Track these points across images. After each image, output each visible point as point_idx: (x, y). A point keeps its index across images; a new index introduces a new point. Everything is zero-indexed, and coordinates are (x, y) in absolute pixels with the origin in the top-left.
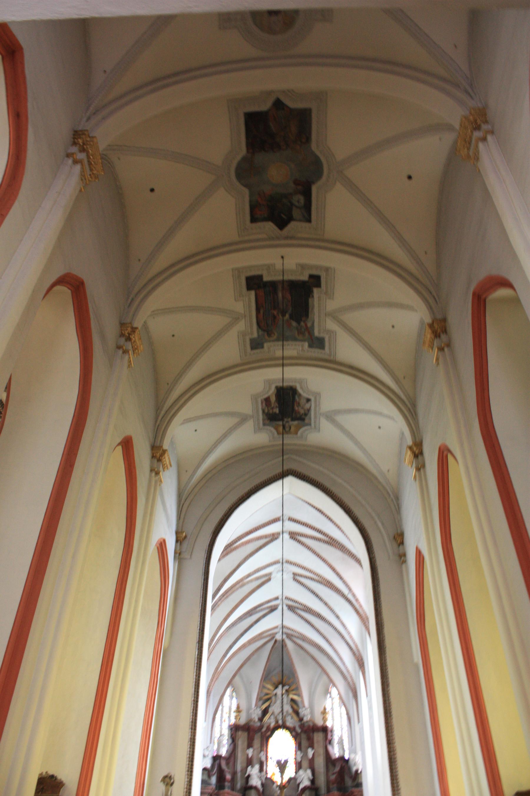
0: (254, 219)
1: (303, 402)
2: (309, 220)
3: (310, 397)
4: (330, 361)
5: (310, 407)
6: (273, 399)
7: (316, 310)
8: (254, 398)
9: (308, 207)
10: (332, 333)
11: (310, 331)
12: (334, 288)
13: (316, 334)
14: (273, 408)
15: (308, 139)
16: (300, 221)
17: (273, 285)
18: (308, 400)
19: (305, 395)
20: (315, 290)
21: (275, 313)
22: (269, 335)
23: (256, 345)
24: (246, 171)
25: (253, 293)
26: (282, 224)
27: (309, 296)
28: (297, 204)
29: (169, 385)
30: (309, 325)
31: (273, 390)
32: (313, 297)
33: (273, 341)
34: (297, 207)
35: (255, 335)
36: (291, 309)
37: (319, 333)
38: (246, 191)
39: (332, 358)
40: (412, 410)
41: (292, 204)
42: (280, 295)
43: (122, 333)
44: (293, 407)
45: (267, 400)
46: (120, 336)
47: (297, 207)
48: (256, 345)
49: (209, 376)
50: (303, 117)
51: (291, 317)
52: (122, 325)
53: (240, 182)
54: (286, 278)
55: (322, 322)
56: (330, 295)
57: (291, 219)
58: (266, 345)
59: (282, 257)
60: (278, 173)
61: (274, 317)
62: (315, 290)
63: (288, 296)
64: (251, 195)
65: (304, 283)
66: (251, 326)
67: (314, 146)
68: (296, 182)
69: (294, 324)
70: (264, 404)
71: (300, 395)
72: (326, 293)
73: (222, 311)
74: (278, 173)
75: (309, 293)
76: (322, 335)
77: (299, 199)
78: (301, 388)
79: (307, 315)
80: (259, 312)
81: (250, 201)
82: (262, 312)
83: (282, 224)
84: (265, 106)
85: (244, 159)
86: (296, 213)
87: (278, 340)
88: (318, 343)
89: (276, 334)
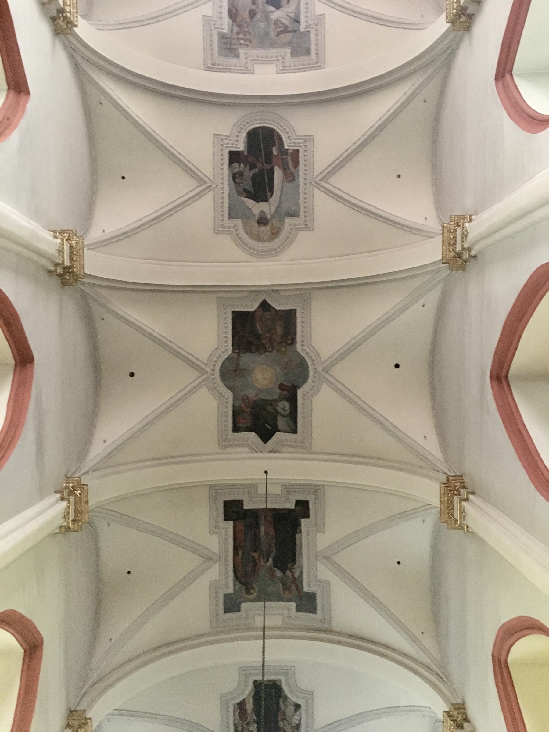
0: (236, 429)
1: (290, 709)
2: (295, 431)
3: (299, 702)
4: (325, 631)
5: (300, 720)
6: (250, 706)
7: (304, 550)
8: (224, 699)
9: (293, 414)
10: (326, 584)
11: (297, 582)
12: (324, 517)
13: (306, 589)
14: (248, 724)
15: (293, 341)
16: (285, 432)
17: (254, 514)
18: (298, 707)
19: (293, 698)
20: (303, 521)
21: (256, 555)
22: (248, 591)
23: (231, 605)
24: (231, 372)
25: (231, 523)
26: (266, 437)
27: (296, 532)
28: (282, 412)
29: (113, 641)
30: (297, 574)
31: (249, 689)
32: (301, 532)
33: (253, 601)
34: (282, 416)
35: (231, 591)
36: (275, 551)
37: (309, 586)
38: (229, 395)
39: (326, 626)
40: (441, 675)
41: (277, 412)
42: (262, 529)
43: (57, 275)
44: (278, 704)
45: (241, 706)
46: (66, 728)
47: (282, 416)
48: (231, 605)
49: (169, 644)
50: (288, 318)
51: (275, 564)
52: (71, 713)
53: (224, 383)
54: (270, 506)
55: (314, 571)
56: (320, 528)
57: (275, 430)
58: (244, 606)
59: (266, 472)
60: (263, 376)
61: (255, 563)
62: (303, 521)
63: (272, 532)
64: (234, 400)
65: (290, 511)
66: (227, 574)
67: (299, 347)
68: (282, 387)
69: (278, 573)
70: (237, 717)
71: (286, 697)
72: (315, 525)
73: (194, 548)
74: (263, 376)
75: (296, 527)
76: (312, 590)
77: (285, 405)
78: (288, 684)
79: (294, 561)
80: (238, 553)
81: (234, 406)
82: (240, 553)
83: (266, 437)
84: (252, 307)
85: (229, 358)
86: (281, 422)
87: (258, 599)
88: (307, 603)
89: (256, 589)
